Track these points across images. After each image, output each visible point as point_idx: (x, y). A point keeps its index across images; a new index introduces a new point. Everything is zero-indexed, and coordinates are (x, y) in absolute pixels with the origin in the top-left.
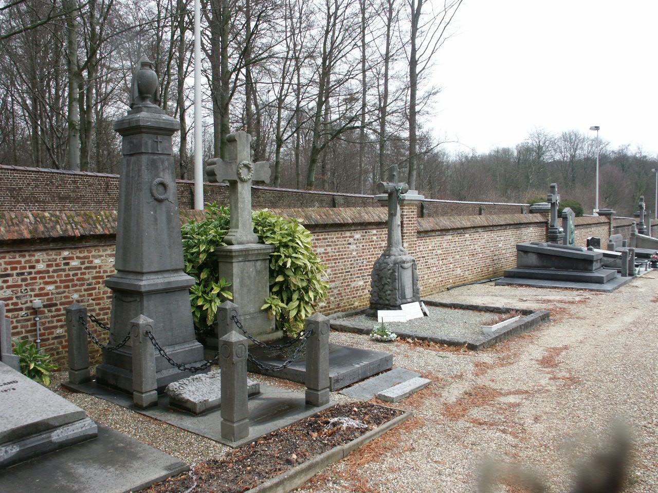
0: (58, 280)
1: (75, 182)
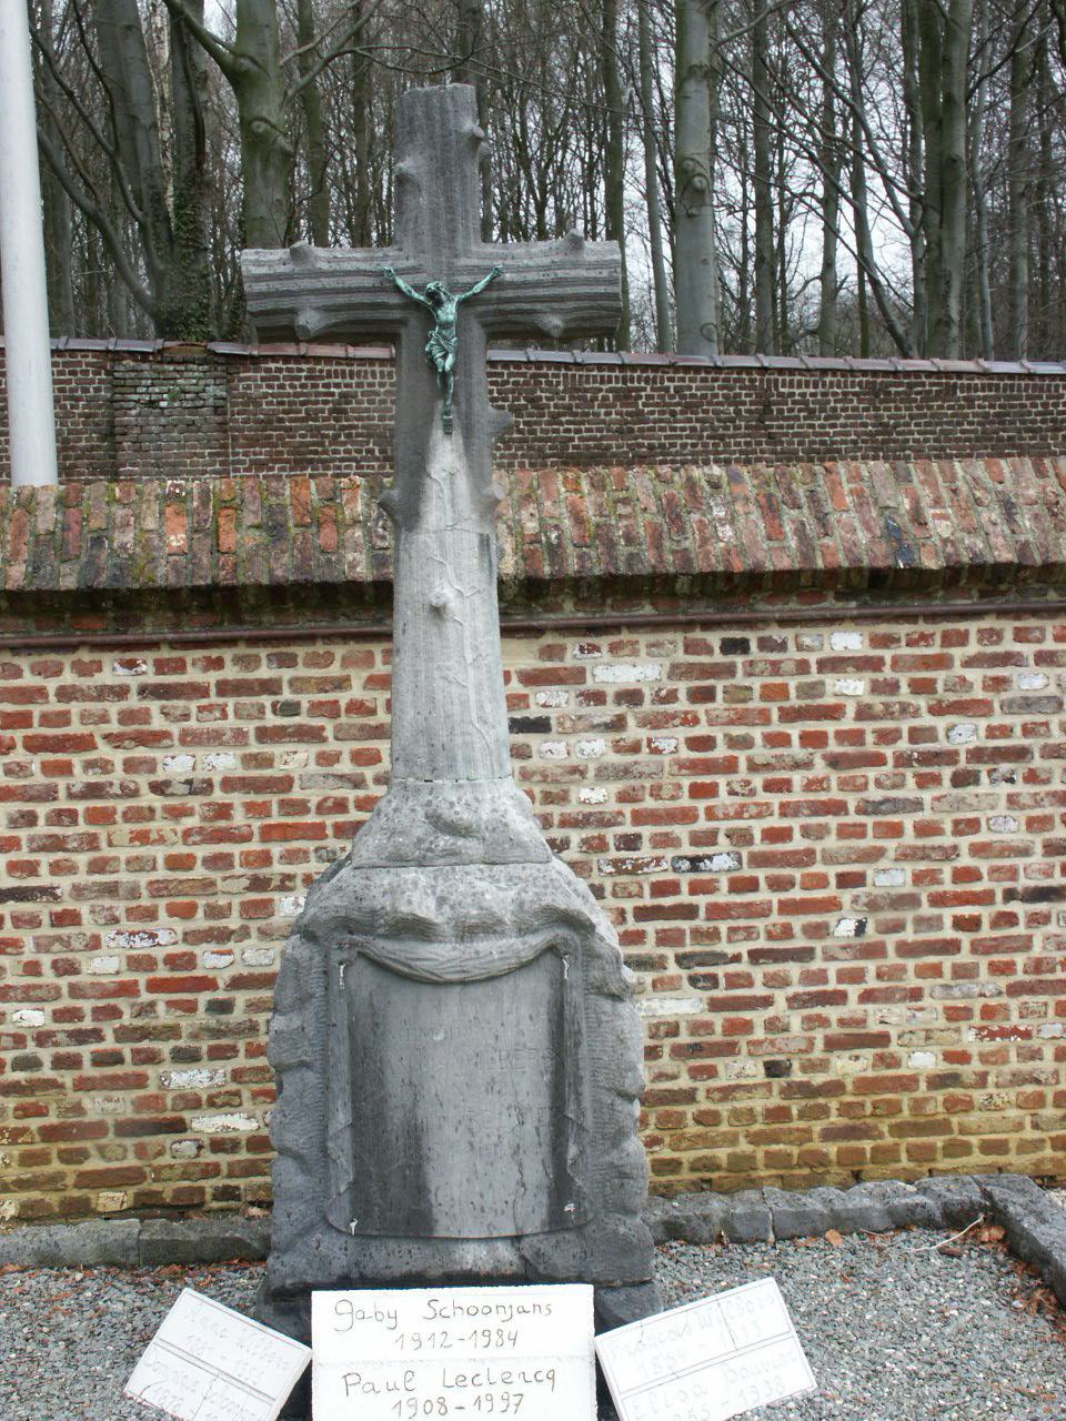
0: (104, 751)
1: (626, 396)
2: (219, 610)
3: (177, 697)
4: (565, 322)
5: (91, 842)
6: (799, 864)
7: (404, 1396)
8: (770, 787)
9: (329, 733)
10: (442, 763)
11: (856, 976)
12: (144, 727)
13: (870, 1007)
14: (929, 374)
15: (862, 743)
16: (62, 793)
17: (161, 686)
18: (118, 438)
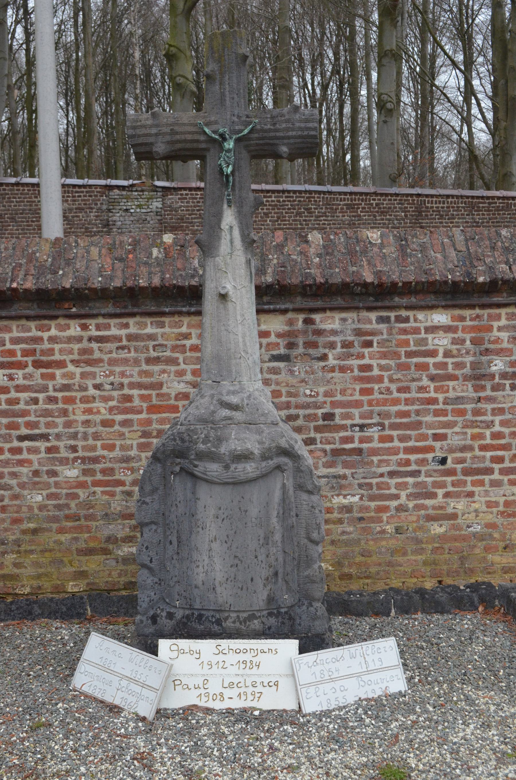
0: (71, 368)
1: (350, 207)
2: (130, 300)
3: (107, 342)
4: (289, 149)
5: (65, 413)
6: (414, 429)
7: (203, 691)
8: (399, 390)
9: (181, 360)
10: (225, 373)
11: (442, 485)
12: (90, 357)
13: (449, 500)
14: (499, 198)
15: (447, 369)
16: (51, 388)
17: (99, 336)
18: (111, 227)
